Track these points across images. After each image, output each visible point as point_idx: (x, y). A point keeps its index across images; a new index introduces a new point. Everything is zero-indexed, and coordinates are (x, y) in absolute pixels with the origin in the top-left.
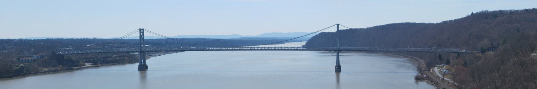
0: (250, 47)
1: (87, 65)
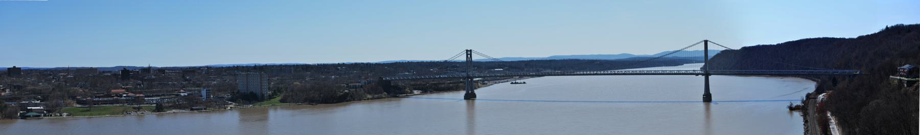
0: (623, 71)
1: (416, 92)
